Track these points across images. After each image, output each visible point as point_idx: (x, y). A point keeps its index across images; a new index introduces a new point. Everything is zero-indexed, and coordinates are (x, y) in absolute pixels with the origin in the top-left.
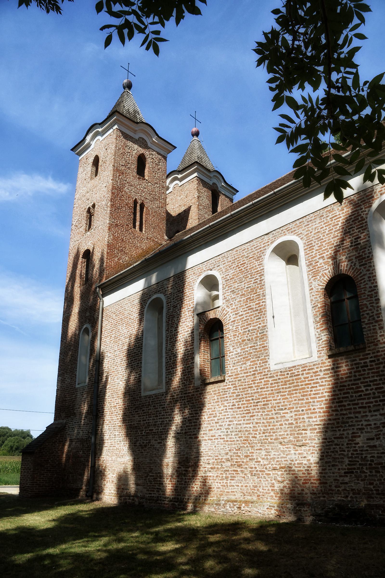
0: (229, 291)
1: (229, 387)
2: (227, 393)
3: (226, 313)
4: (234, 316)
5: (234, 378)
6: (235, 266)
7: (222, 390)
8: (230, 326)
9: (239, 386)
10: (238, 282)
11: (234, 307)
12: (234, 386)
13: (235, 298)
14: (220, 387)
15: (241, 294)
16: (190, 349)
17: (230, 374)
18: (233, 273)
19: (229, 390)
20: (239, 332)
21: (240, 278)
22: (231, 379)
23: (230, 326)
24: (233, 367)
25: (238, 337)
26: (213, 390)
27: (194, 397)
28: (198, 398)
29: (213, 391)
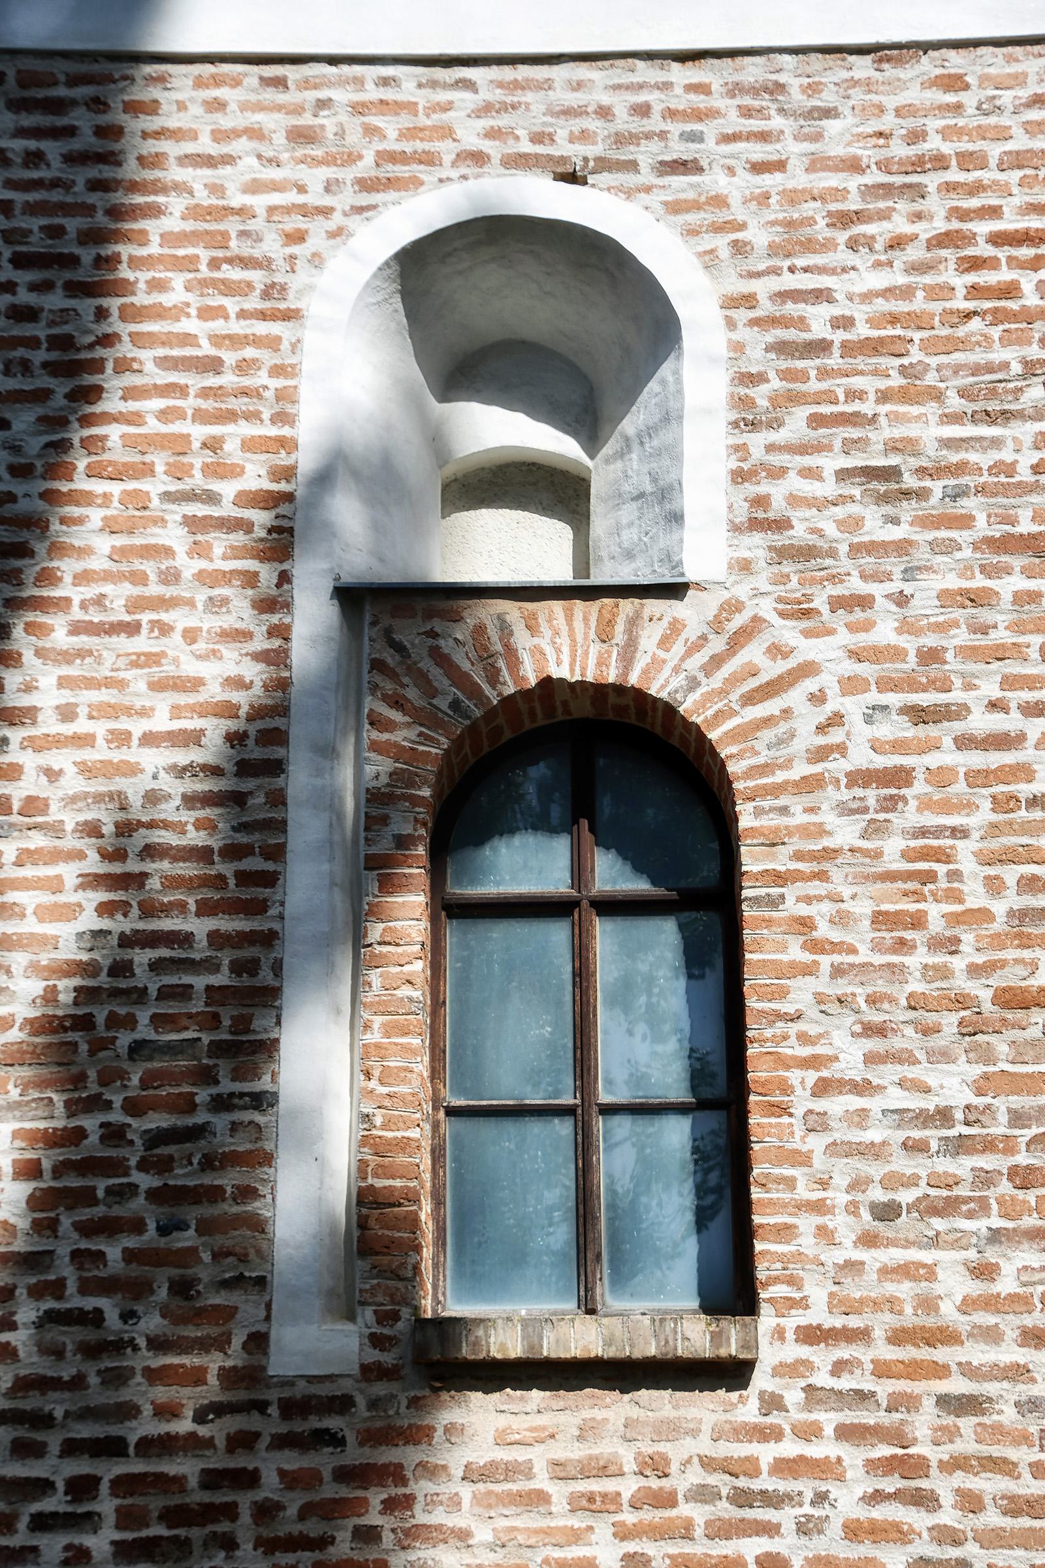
0: (831, 463)
1: (815, 1450)
2: (786, 1517)
3: (772, 669)
4: (895, 728)
5: (882, 1370)
6: (925, 231)
7: (696, 1476)
8: (828, 818)
9: (957, 1464)
10: (955, 402)
11: (885, 632)
12: (884, 1451)
13: (903, 547)
14: (672, 1430)
15: (982, 527)
16: (216, 938)
17: (819, 1315)
18: (888, 293)
19: (806, 1487)
20: (955, 896)
21: (976, 370)
22: (839, 1368)
23: (828, 818)
24: (868, 1240)
25: (951, 945)
26: (570, 1451)
27: (245, 1501)
28: (313, 1528)
29: (560, 1471)
